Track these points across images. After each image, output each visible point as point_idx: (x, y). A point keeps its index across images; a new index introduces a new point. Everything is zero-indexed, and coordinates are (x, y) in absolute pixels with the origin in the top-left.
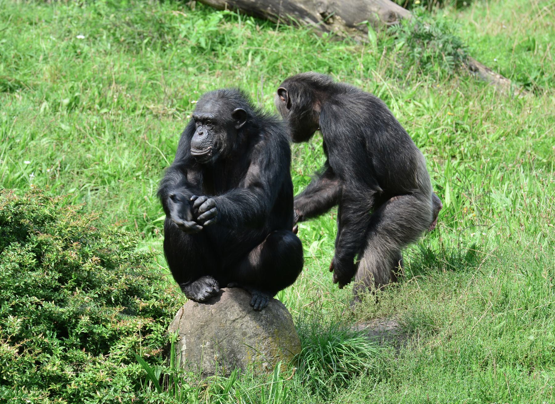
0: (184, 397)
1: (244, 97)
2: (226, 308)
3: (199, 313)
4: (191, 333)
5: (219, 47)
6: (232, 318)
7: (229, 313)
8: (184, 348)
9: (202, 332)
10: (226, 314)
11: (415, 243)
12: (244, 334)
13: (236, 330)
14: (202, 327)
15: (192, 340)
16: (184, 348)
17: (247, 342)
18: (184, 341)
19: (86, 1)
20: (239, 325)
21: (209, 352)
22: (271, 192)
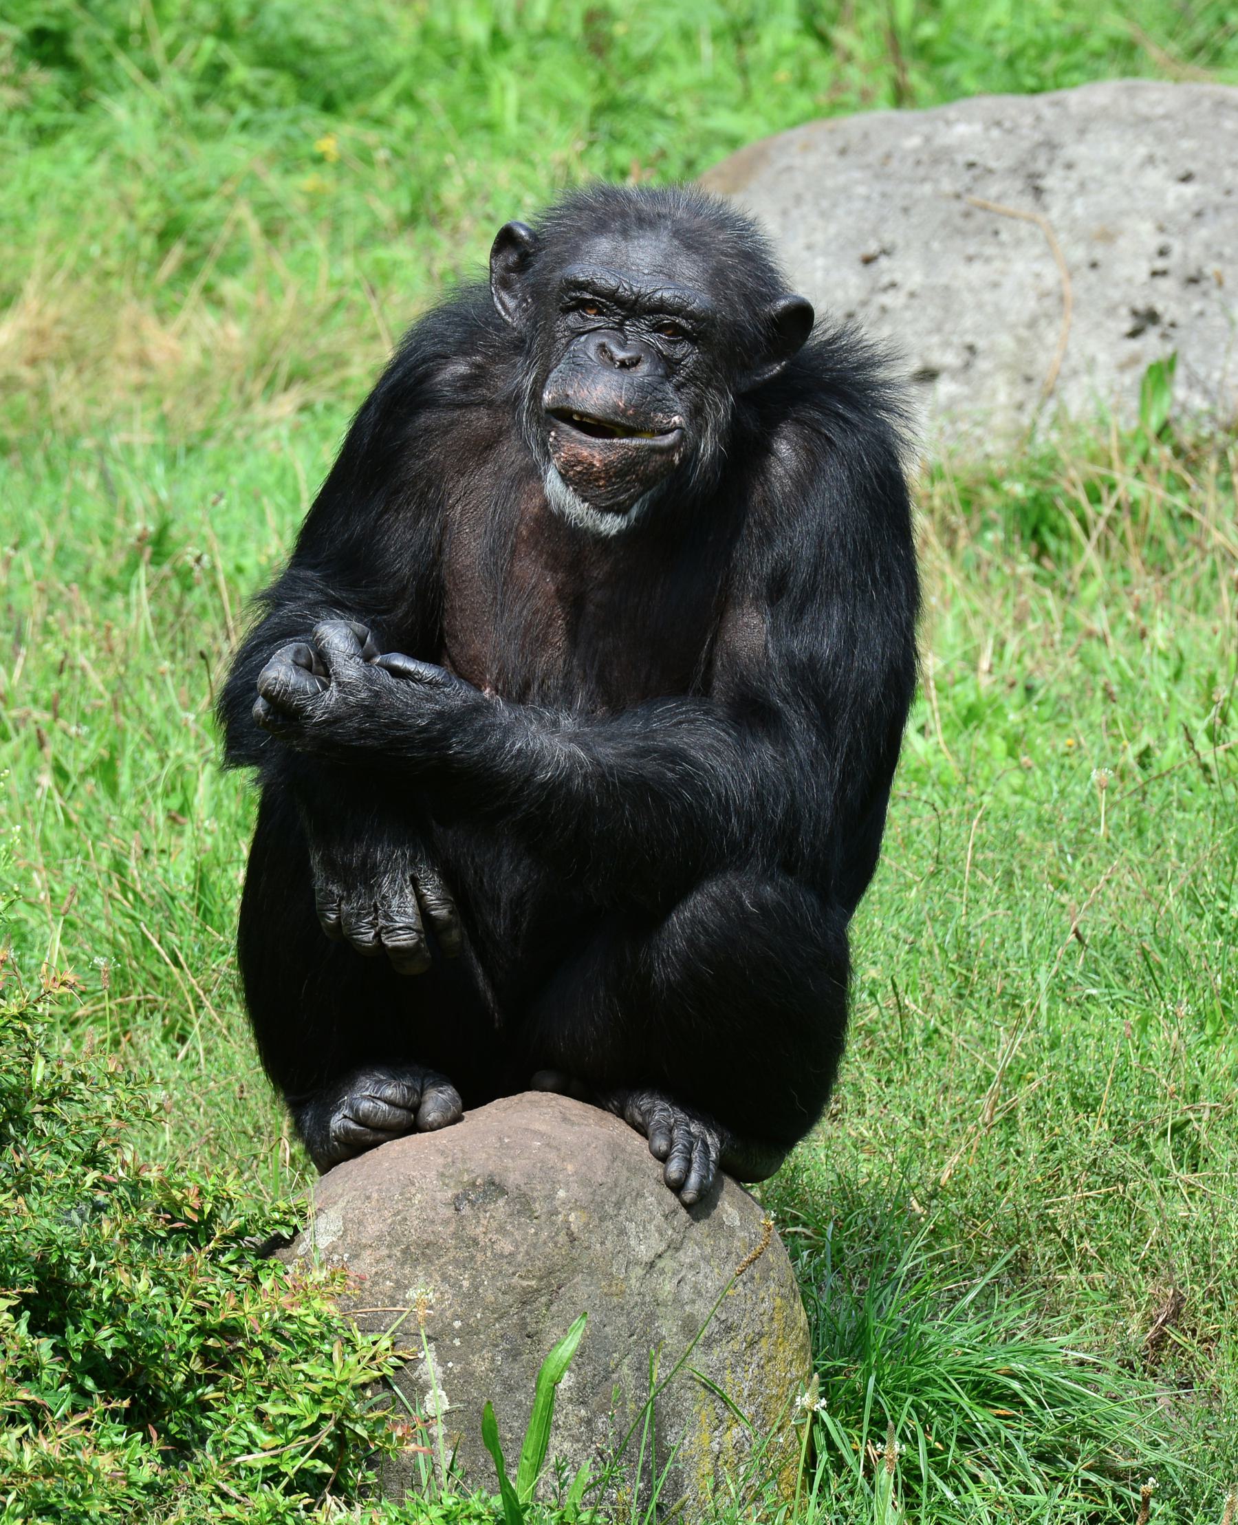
1: (616, 413)
2: (618, 1205)
3: (501, 1230)
4: (469, 1332)
6: (644, 1252)
7: (631, 1227)
8: (437, 1402)
9: (523, 1324)
10: (622, 1232)
11: (1016, 499)
12: (689, 1327)
13: (661, 1310)
14: (526, 1299)
15: (480, 1365)
16: (437, 1402)
17: (700, 1362)
18: (430, 1368)
19: (1182, 17)
20: (668, 1287)
21: (572, 1420)
22: (883, 422)
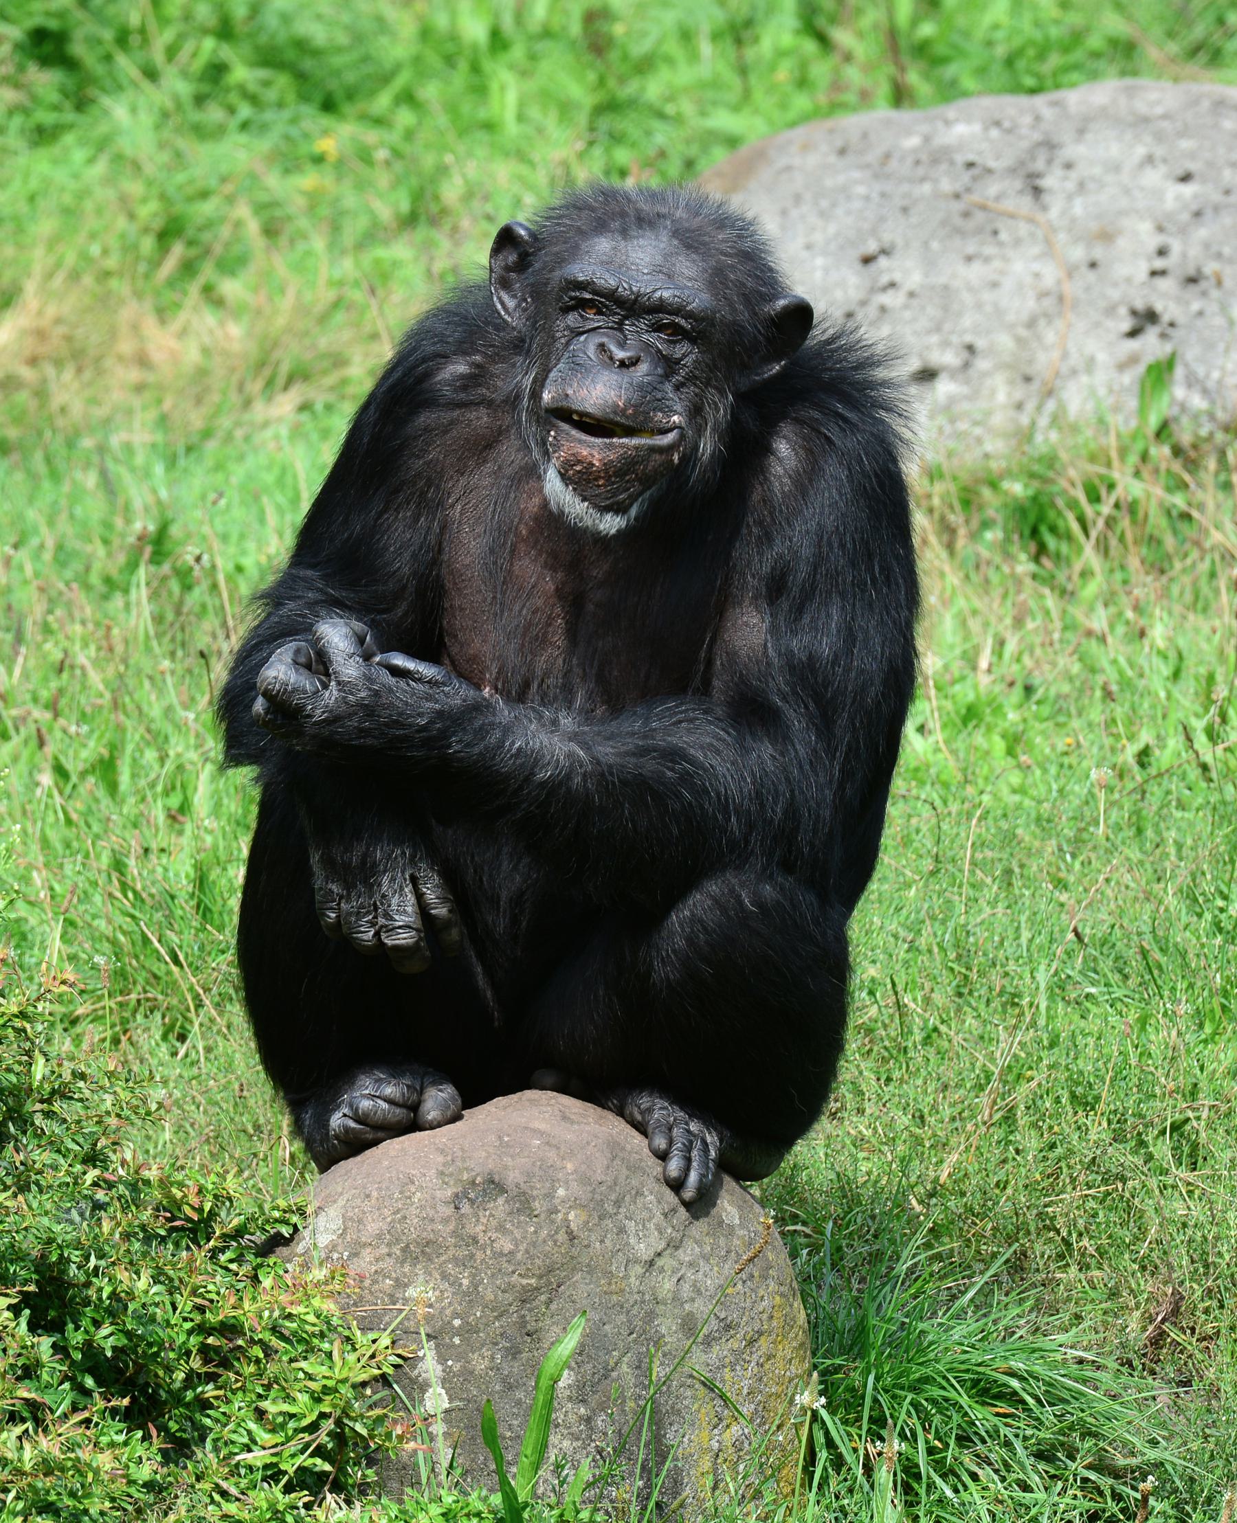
0: (162, 1278)
2: (618, 1203)
3: (501, 1228)
4: (468, 1330)
5: (1157, 888)
6: (643, 1250)
7: (630, 1225)
8: (436, 1400)
9: (523, 1323)
10: (622, 1230)
11: (1015, 499)
12: (689, 1326)
13: (660, 1309)
14: (526, 1297)
15: (480, 1364)
16: (436, 1400)
17: (699, 1361)
18: (430, 1366)
20: (668, 1285)
21: (572, 1418)
22: (882, 422)
